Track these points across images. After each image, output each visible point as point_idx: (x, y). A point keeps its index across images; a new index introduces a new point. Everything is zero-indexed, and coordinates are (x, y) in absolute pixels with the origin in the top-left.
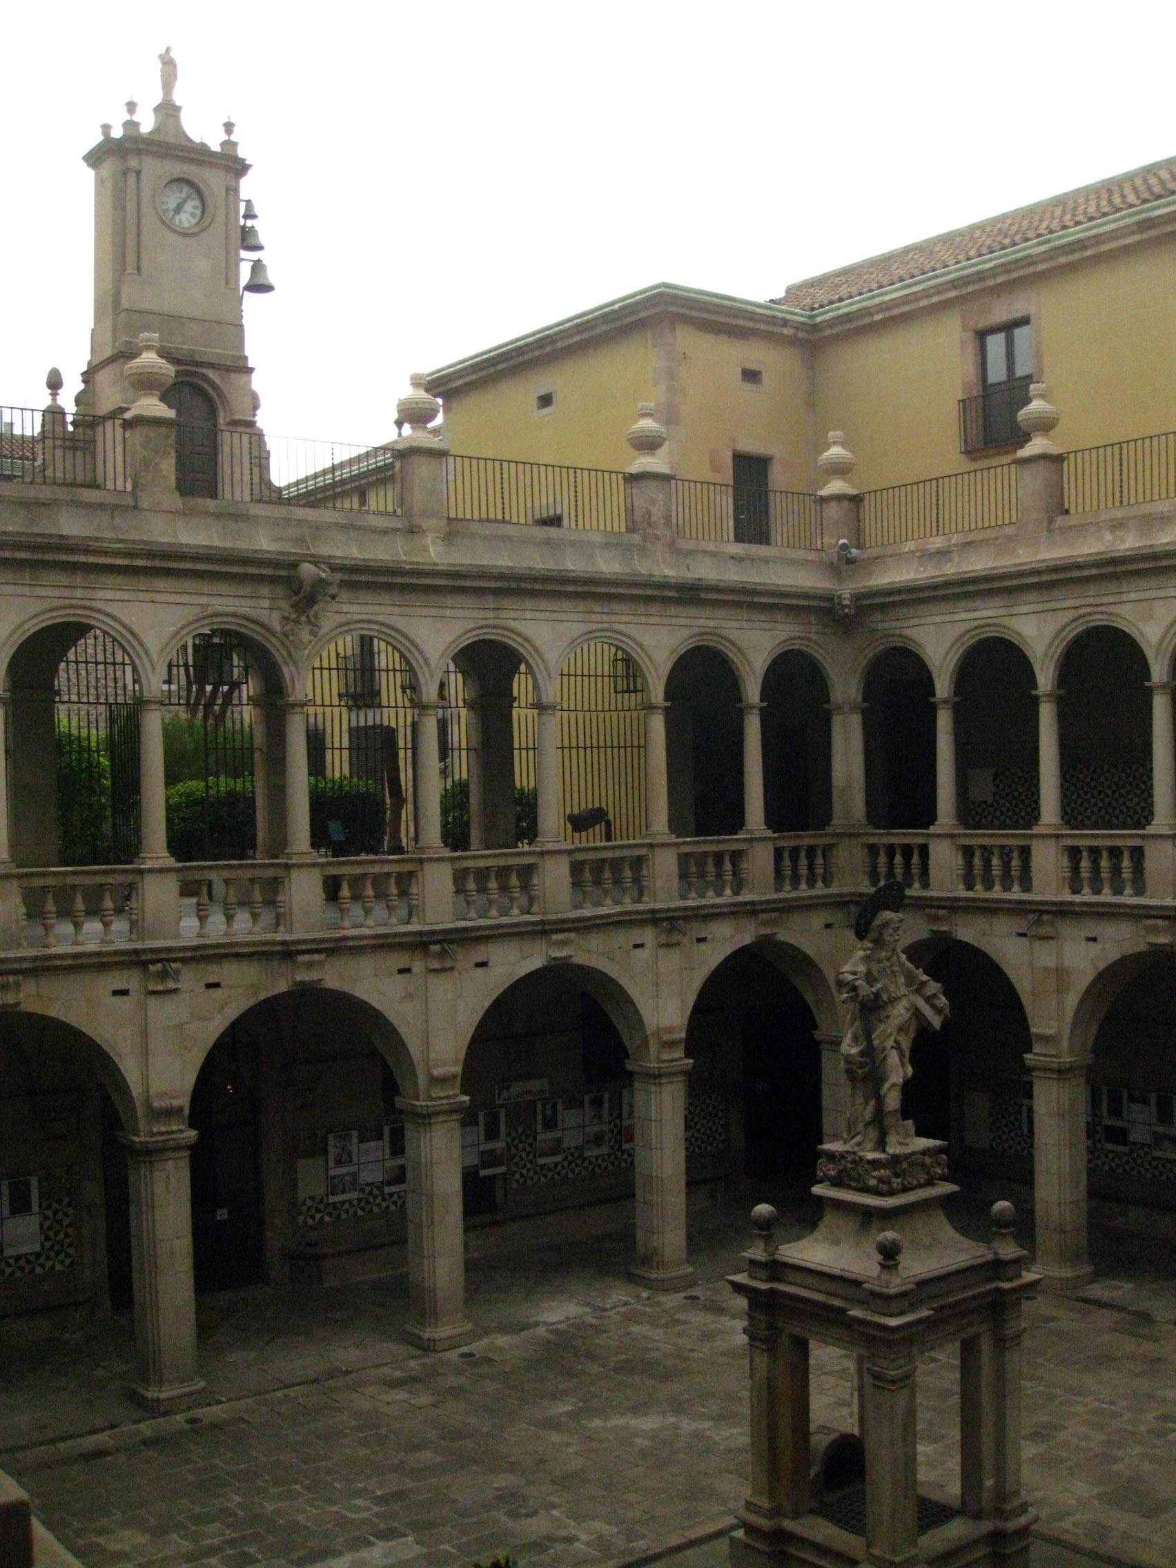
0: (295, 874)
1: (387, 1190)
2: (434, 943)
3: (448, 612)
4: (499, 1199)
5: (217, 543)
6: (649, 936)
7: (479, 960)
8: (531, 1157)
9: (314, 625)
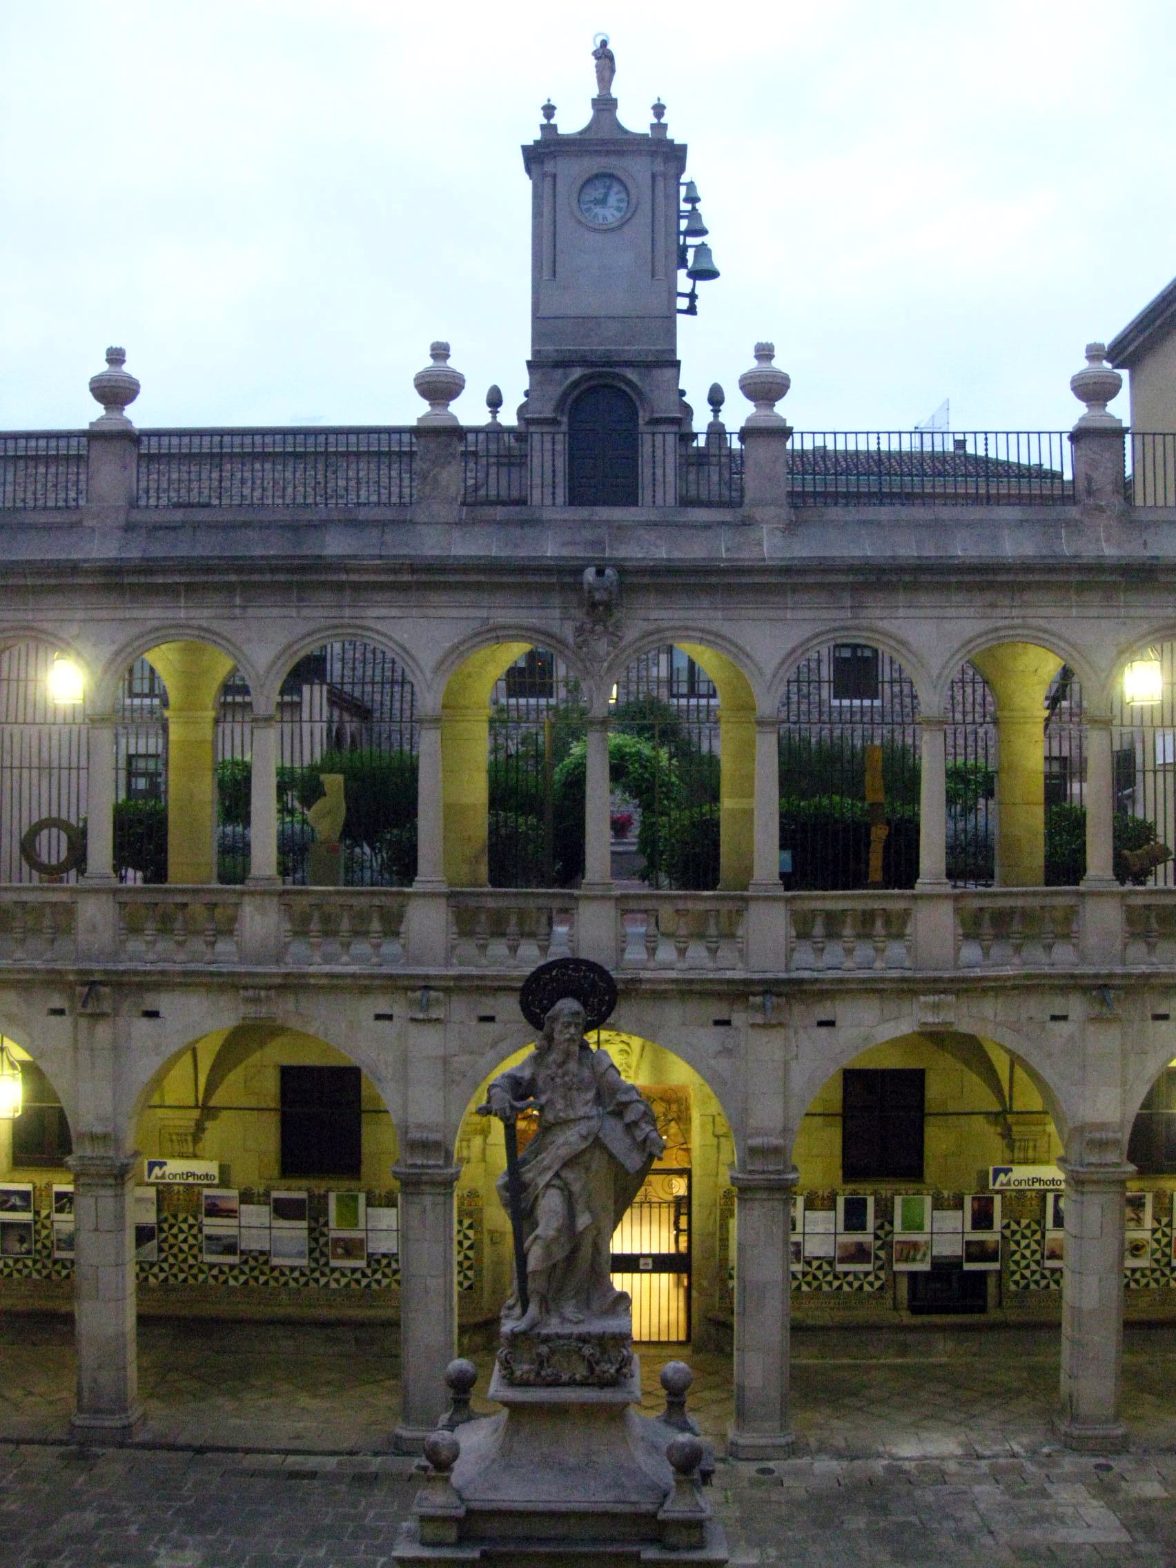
0: (753, 906)
1: (841, 1268)
2: (754, 995)
3: (789, 615)
4: (991, 1300)
5: (494, 552)
6: (1076, 1006)
7: (824, 1018)
8: (1038, 1256)
9: (614, 635)
